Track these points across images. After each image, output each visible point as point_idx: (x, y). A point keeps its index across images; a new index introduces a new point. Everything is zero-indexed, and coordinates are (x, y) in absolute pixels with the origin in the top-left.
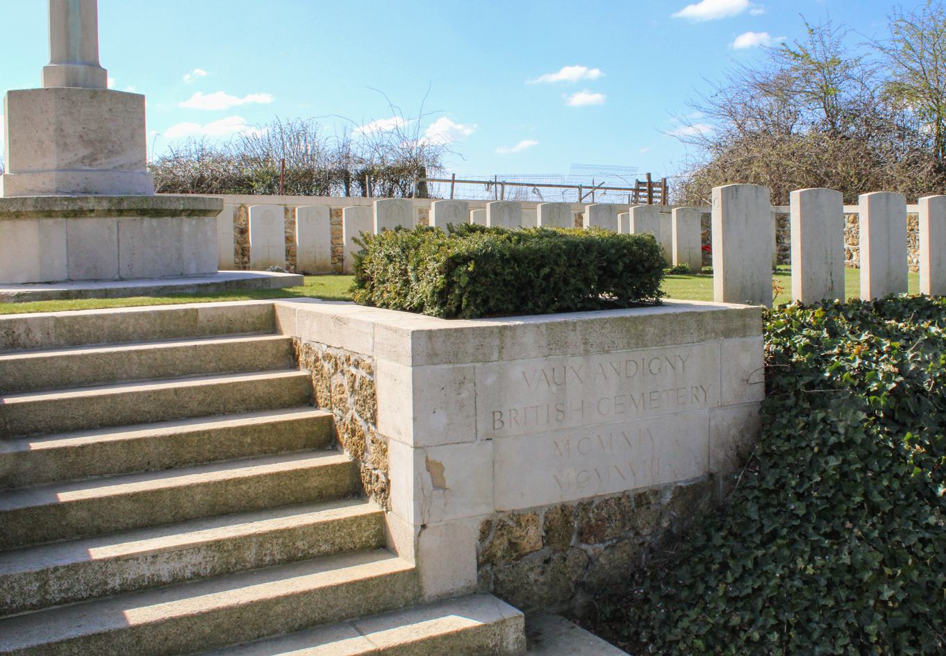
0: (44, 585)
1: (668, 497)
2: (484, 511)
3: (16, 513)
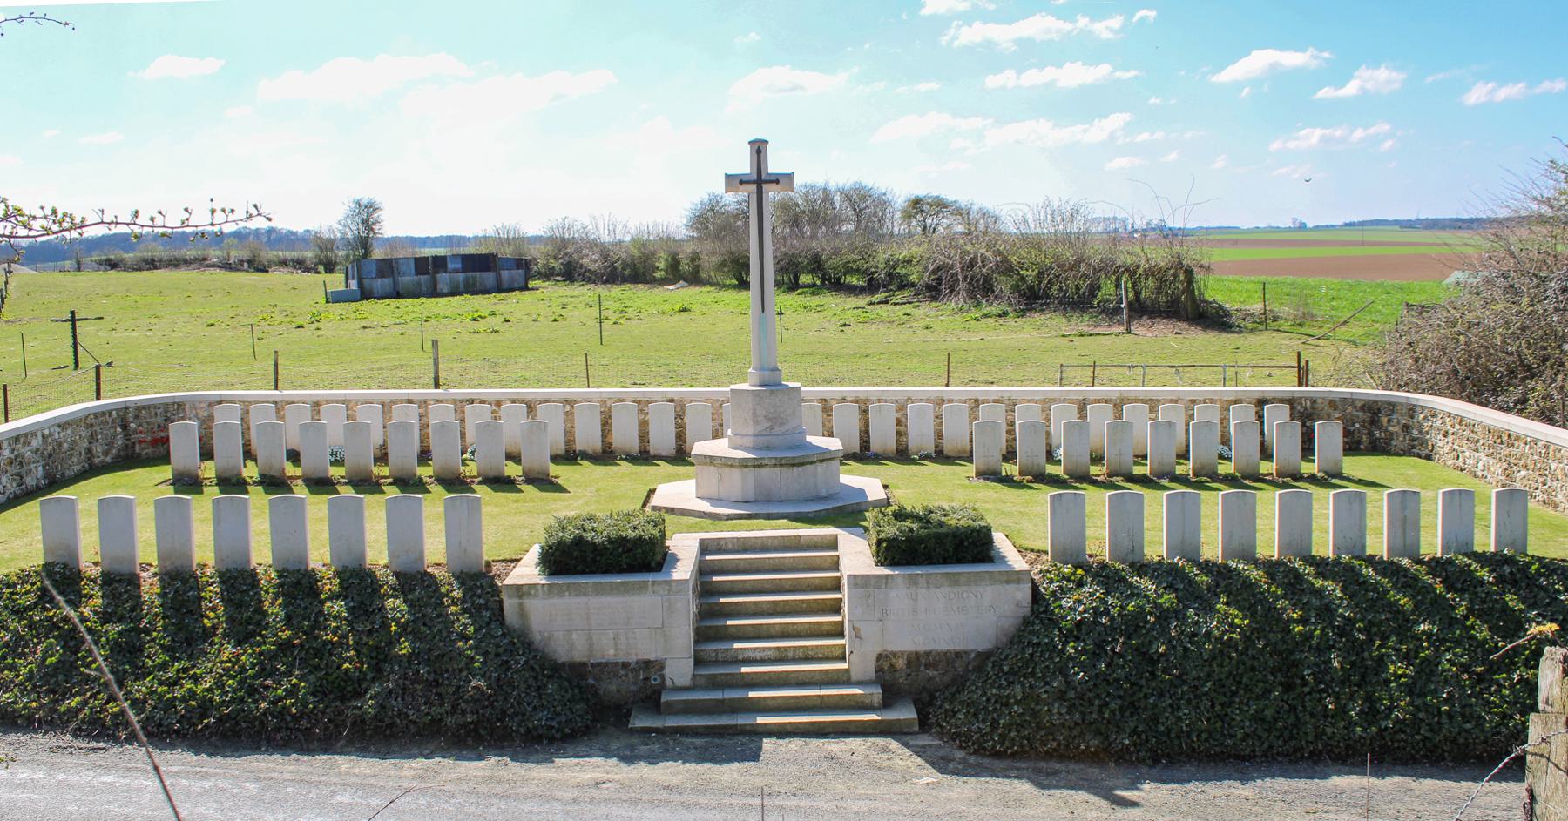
0: (717, 655)
1: (973, 655)
2: (879, 650)
3: (711, 627)
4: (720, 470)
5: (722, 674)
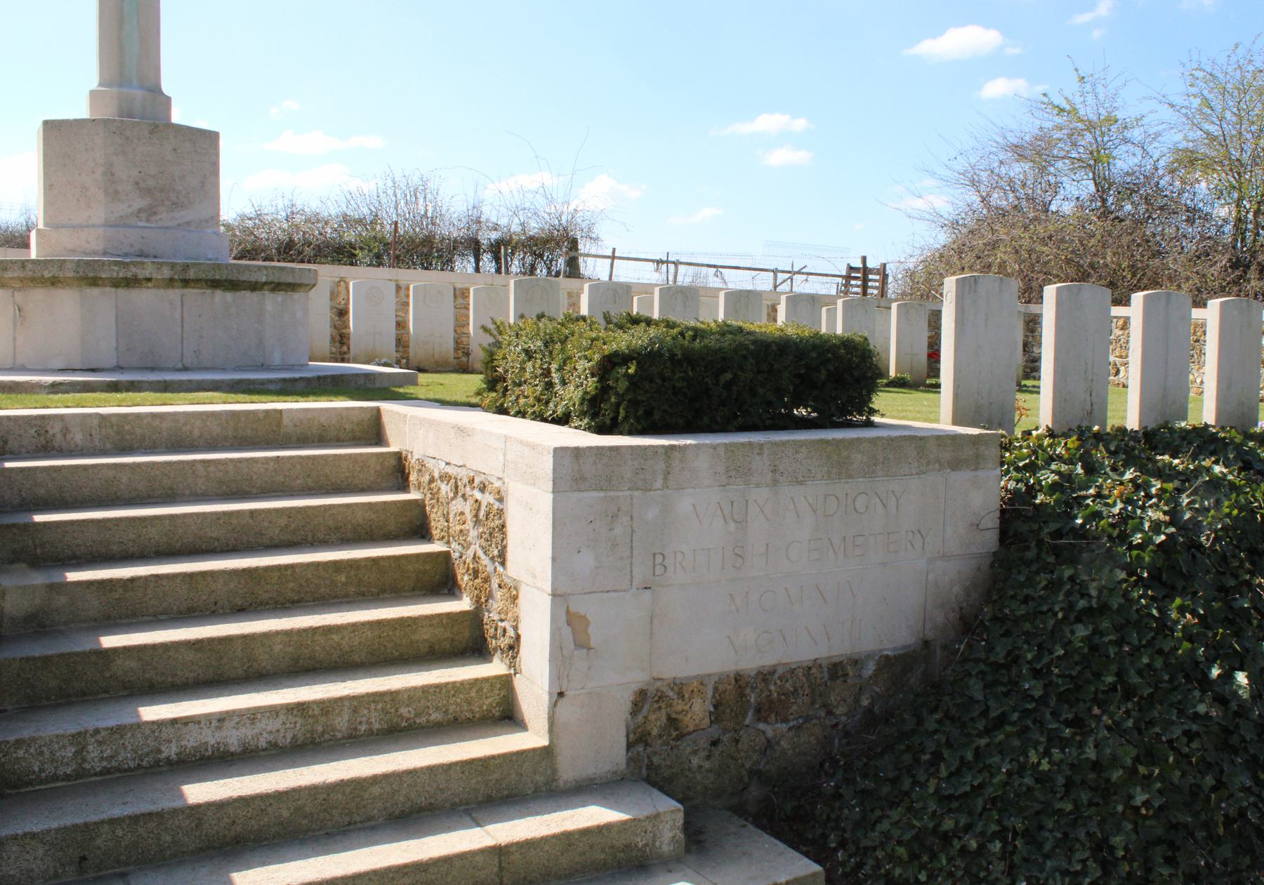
2: (637, 678)
3: (47, 660)
4: (19, 297)
5: (113, 822)
